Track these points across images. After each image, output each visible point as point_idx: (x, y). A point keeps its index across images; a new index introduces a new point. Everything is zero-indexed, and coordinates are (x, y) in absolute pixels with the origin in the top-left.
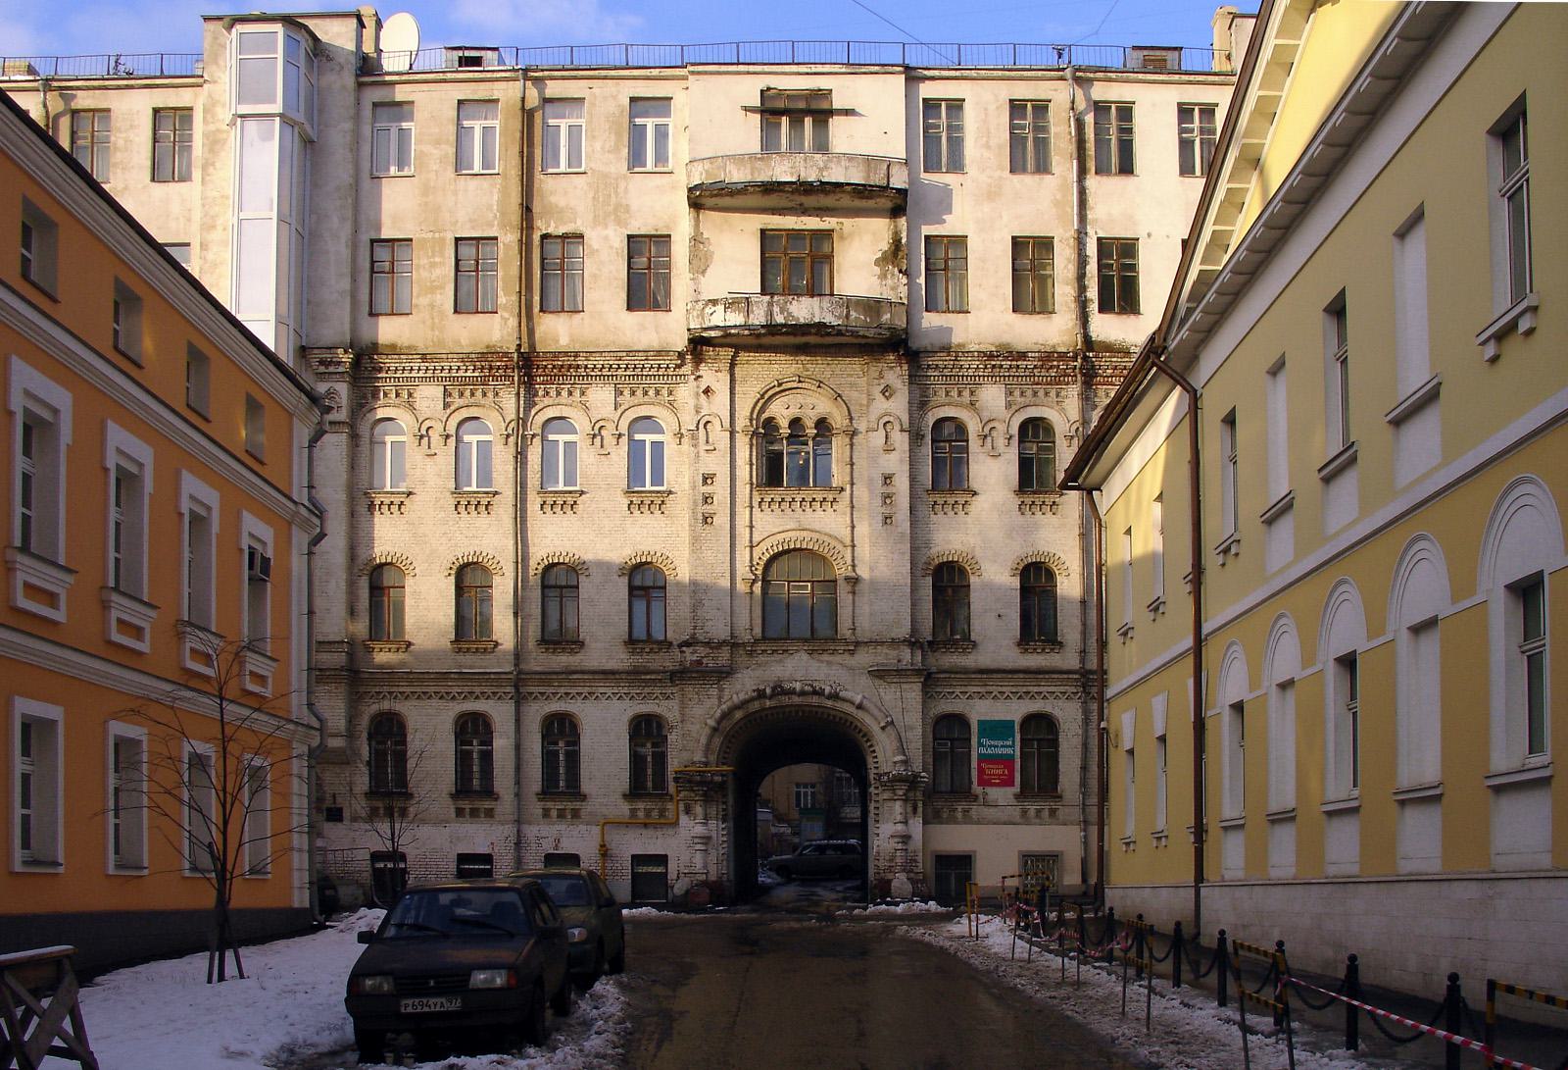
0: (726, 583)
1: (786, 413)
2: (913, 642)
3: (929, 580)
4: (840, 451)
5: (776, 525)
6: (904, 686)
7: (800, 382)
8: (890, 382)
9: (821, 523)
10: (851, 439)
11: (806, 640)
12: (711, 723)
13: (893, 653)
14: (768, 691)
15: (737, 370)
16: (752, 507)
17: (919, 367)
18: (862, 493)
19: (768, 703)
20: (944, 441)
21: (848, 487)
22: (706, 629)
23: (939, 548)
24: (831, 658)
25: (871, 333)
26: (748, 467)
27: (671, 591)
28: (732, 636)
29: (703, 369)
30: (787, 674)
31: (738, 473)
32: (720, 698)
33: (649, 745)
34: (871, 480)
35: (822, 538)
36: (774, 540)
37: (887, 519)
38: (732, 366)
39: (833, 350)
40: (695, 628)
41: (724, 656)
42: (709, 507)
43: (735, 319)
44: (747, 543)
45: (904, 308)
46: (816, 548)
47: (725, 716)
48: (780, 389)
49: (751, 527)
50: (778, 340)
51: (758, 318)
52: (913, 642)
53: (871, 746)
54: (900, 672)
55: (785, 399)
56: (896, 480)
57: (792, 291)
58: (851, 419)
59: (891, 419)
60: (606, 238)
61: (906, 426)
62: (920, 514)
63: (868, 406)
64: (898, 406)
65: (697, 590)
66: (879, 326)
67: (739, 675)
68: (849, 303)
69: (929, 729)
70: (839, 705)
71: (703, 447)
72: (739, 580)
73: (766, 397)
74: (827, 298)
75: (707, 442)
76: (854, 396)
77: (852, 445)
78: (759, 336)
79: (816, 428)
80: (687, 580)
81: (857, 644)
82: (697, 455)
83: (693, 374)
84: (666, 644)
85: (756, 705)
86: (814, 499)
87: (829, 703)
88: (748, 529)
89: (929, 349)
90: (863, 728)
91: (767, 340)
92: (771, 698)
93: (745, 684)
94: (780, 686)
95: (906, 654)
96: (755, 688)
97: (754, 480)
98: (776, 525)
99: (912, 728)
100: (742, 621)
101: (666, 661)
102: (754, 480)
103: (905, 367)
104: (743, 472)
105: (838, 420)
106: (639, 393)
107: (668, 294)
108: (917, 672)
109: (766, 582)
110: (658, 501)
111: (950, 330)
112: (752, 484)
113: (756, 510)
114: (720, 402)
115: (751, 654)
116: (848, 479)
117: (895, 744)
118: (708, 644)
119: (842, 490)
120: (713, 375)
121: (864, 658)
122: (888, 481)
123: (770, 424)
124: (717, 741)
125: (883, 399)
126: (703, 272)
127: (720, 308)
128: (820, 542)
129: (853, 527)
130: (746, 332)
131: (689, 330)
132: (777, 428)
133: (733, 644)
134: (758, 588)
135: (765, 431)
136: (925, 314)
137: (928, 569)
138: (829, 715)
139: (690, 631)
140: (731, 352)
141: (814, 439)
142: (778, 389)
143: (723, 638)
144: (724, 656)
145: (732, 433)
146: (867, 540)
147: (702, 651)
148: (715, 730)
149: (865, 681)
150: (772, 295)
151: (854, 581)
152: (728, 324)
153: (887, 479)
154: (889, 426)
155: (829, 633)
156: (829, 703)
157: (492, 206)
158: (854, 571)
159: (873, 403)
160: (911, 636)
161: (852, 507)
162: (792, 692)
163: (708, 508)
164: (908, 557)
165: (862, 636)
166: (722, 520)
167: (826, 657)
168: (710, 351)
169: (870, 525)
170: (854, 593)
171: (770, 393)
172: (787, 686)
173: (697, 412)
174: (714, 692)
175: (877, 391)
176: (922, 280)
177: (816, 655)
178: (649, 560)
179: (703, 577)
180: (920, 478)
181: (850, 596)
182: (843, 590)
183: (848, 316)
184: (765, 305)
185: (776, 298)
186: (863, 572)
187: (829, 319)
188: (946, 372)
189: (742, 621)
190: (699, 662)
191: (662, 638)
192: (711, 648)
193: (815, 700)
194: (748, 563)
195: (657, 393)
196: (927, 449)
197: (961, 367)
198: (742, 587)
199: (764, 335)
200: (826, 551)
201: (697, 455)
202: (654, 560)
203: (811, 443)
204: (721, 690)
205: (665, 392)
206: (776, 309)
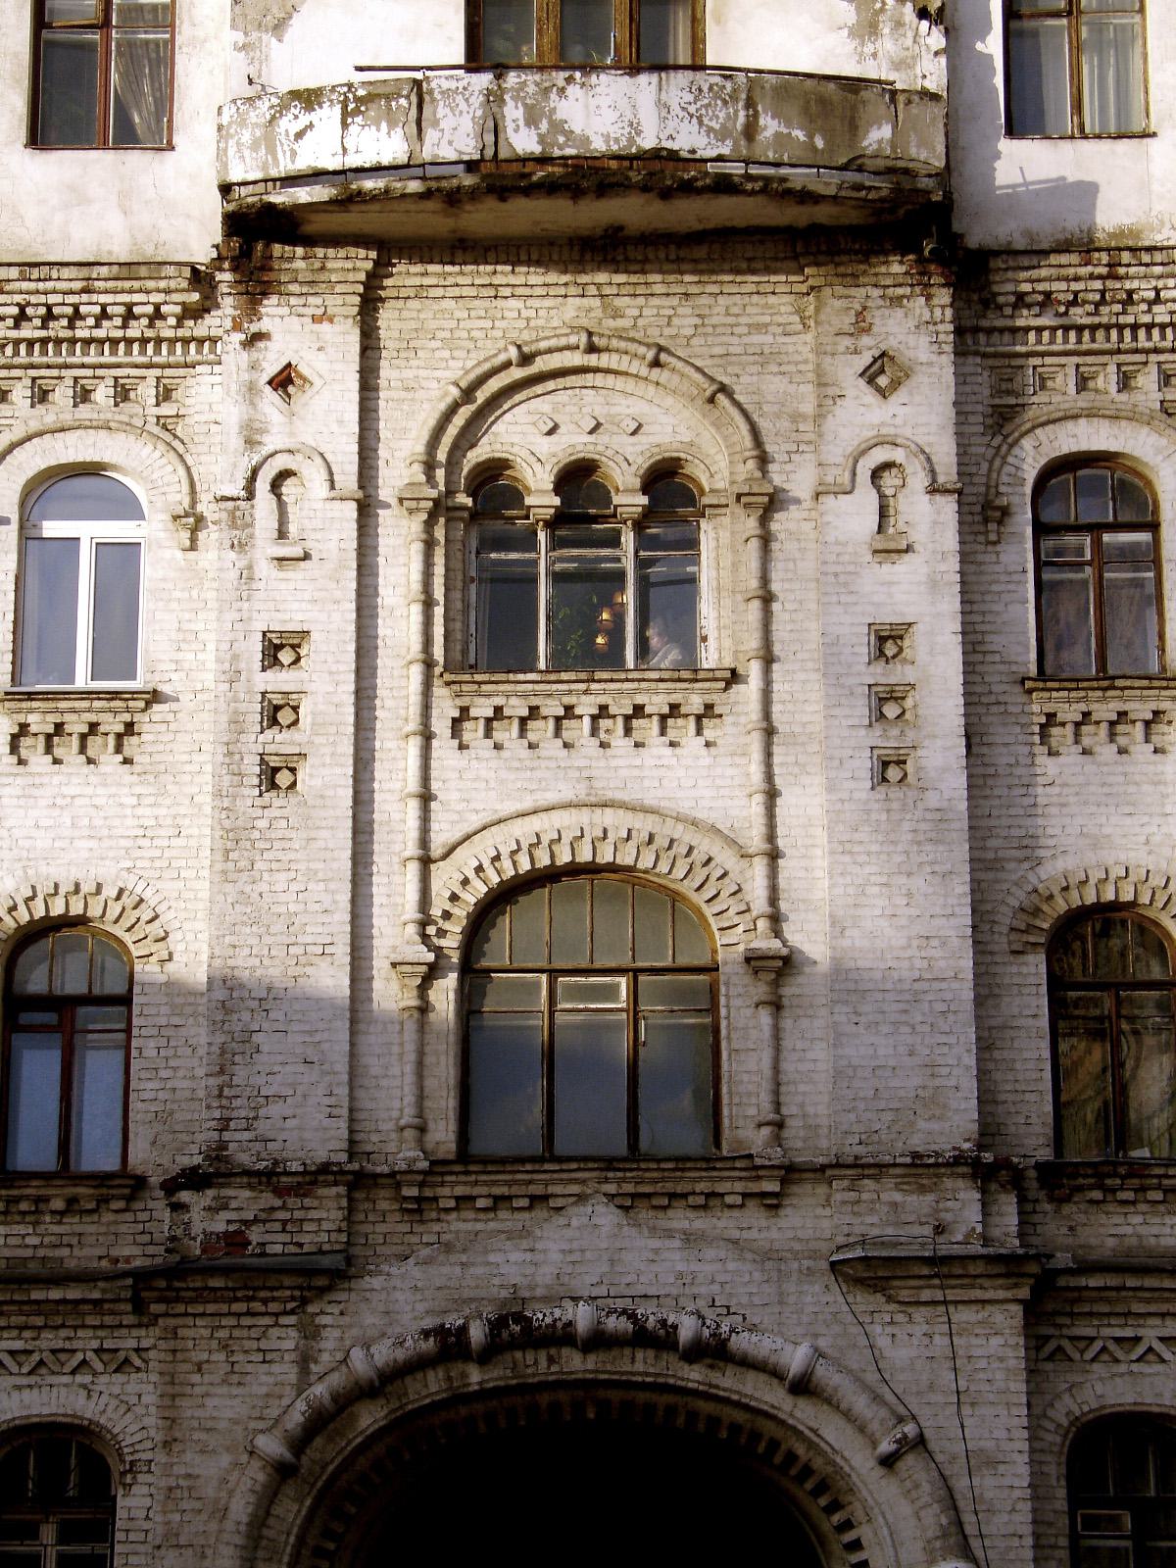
0: (332, 979)
1: (545, 446)
2: (987, 1167)
3: (1036, 966)
4: (726, 561)
5: (507, 792)
6: (963, 1316)
7: (592, 349)
8: (891, 344)
9: (668, 784)
10: (764, 520)
11: (609, 1163)
12: (272, 1446)
13: (918, 1204)
14: (477, 1333)
15: (388, 319)
16: (427, 736)
17: (989, 303)
18: (802, 697)
19: (475, 1376)
20: (1077, 529)
21: (754, 670)
22: (262, 1127)
23: (1061, 865)
24: (700, 1223)
25: (827, 183)
26: (416, 610)
27: (146, 1014)
28: (353, 1148)
29: (273, 314)
30: (545, 1276)
31: (385, 628)
32: (305, 1361)
33: (48, 1533)
34: (831, 646)
35: (666, 830)
36: (501, 839)
37: (888, 768)
38: (369, 304)
39: (701, 252)
40: (224, 1124)
41: (323, 1219)
42: (286, 735)
43: (379, 144)
44: (412, 849)
45: (938, 111)
46: (647, 862)
47: (319, 1422)
48: (528, 374)
49: (426, 798)
50: (525, 214)
51: (453, 138)
52: (987, 1167)
53: (835, 1506)
54: (943, 1267)
55: (543, 405)
56: (917, 645)
57: (577, 55)
58: (763, 460)
59: (898, 455)
61: (948, 473)
62: (1002, 758)
63: (819, 417)
64: (924, 415)
65: (235, 1007)
66: (855, 164)
67: (376, 1282)
68: (757, 89)
69: (1055, 1470)
70: (728, 1381)
71: (265, 545)
72: (380, 966)
73: (481, 396)
74: (681, 78)
75: (282, 534)
76: (771, 392)
77: (766, 540)
78: (453, 198)
79: (645, 489)
80: (200, 976)
81: (791, 1173)
82: (247, 576)
83: (237, 327)
84: (127, 1185)
85: (432, 1385)
86: (639, 711)
87: (694, 1375)
88: (414, 805)
89: (1020, 244)
90: (818, 1463)
91: (484, 218)
92: (486, 1356)
93: (393, 1310)
94: (519, 1318)
95: (964, 1207)
96: (429, 1323)
97: (438, 652)
98: (507, 792)
99: (992, 1463)
100: (391, 1100)
101: (125, 1240)
102: (438, 652)
103: (943, 296)
104: (401, 627)
105: (718, 466)
106: (62, 395)
107: (164, 103)
108: (1007, 1266)
109: (473, 975)
110: (108, 719)
111: (1087, 192)
112: (429, 664)
113: (443, 746)
114: (328, 415)
115: (418, 1209)
116: (753, 642)
117: (934, 1518)
118: (268, 1177)
119: (734, 677)
120: (310, 331)
121: (815, 1220)
122: (890, 649)
123: (493, 485)
124: (291, 1511)
125: (869, 396)
126: (279, 28)
127: (328, 116)
128: (661, 842)
129: (772, 795)
130: (414, 186)
131: (226, 189)
132: (514, 496)
133: (357, 1178)
134: (445, 993)
135: (477, 506)
136: (1006, 145)
137: (1030, 929)
138: (693, 1415)
139: (207, 1136)
140: (363, 260)
141: (639, 526)
142: (517, 373)
143: (321, 1156)
144: (325, 1214)
145: (366, 509)
146: (821, 836)
147: (245, 1201)
148: (283, 1472)
149: (820, 1297)
150: (500, 70)
151: (777, 969)
152: (353, 161)
153: (888, 640)
154: (889, 480)
155: (692, 1141)
156: (694, 1375)
158: (777, 933)
159: (837, 418)
160: (981, 1147)
161: (769, 732)
162: (562, 1337)
163: (280, 741)
164: (961, 887)
165: (801, 1145)
166: (326, 776)
167: (680, 1219)
168: (294, 260)
169: (831, 788)
170: (777, 1006)
171: (494, 384)
172: (542, 1316)
173: (251, 443)
174: (285, 1339)
175: (848, 370)
176: (993, 45)
177: (644, 1214)
178: (76, 909)
179: (260, 962)
180: (996, 642)
181: (765, 1017)
182: (743, 1017)
183: (750, 131)
184: (477, 100)
185: (512, 79)
186: (808, 936)
187: (688, 139)
188: (1078, 315)
189: (391, 1100)
190: (235, 1240)
191: (112, 1164)
192: (279, 1192)
193: (641, 1364)
194: (411, 911)
195: (122, 394)
196: (1019, 551)
197: (1129, 300)
198: (390, 994)
199: (474, 194)
200: (679, 872)
201: (247, 576)
202: (94, 911)
203: (628, 539)
204: (311, 1332)
205: (147, 391)
206: (513, 112)
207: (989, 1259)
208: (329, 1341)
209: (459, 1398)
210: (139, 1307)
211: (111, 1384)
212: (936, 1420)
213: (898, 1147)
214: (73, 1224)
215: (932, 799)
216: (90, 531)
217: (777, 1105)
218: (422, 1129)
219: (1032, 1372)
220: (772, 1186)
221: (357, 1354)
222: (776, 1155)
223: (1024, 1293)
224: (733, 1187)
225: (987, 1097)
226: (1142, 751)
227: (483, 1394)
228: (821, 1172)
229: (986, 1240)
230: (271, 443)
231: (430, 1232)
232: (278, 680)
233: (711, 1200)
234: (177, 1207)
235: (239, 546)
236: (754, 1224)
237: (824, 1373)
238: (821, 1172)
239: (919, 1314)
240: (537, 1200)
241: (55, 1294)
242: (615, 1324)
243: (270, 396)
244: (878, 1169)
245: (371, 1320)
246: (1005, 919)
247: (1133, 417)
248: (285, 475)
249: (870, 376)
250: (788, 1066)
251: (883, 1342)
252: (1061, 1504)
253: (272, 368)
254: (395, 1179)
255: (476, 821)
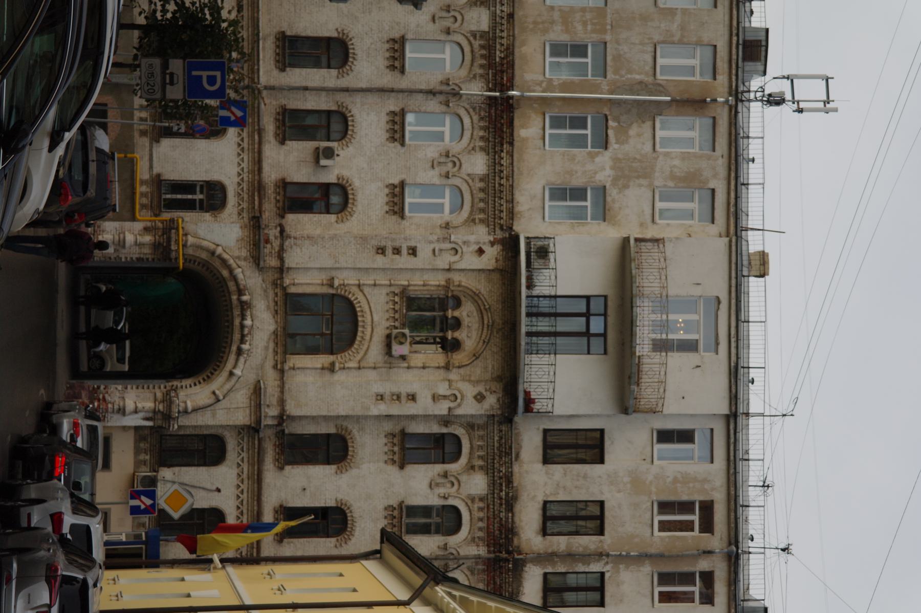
2: (282, 418)
3: (332, 430)
6: (248, 411)
12: (219, 250)
13: (274, 401)
17: (500, 423)
22: (294, 247)
24: (271, 350)
28: (289, 269)
32: (239, 258)
33: (201, 197)
40: (295, 238)
47: (224, 262)
52: (282, 418)
53: (204, 380)
56: (411, 404)
59: (459, 400)
60: (603, 169)
70: (232, 357)
71: (437, 246)
75: (441, 250)
77: (438, 368)
81: (282, 372)
82: (431, 242)
85: (232, 286)
92: (239, 299)
93: (251, 279)
95: (274, 412)
105: (458, 357)
108: (259, 421)
115: (275, 284)
118: (282, 250)
123: (458, 303)
124: (204, 255)
125: (474, 393)
133: (282, 270)
139: (293, 234)
144: (273, 262)
147: (276, 244)
148: (213, 253)
149: (251, 378)
157: (631, 74)
158: (340, 369)
162: (243, 317)
163: (389, 251)
167: (272, 345)
170: (323, 369)
173: (464, 243)
177: (273, 337)
181: (320, 366)
190: (267, 241)
193: (237, 336)
196: (436, 429)
201: (431, 242)
207: (260, 417)
208: (242, 263)
209: (229, 293)
210: (254, 217)
211: (235, 211)
212: (224, 404)
213: (287, 396)
214: (273, 201)
215: (372, 407)
216: (446, 201)
217: (298, 368)
218: (294, 284)
219: (236, 426)
220: (279, 366)
221: (240, 270)
222: (286, 368)
223: (253, 425)
224: (279, 358)
225: (301, 418)
226: (386, 458)
227: (230, 300)
228: (282, 379)
229: (265, 417)
230: (465, 249)
231: (269, 286)
232: (404, 251)
233: (276, 353)
234: (276, 227)
235: (438, 240)
236: (270, 363)
237: (234, 379)
238: (282, 379)
239: (248, 401)
240: (276, 312)
241: (256, 198)
242: (246, 331)
243: (477, 247)
244: (282, 392)
245: (248, 273)
246: (345, 424)
247: (470, 459)
248: (457, 251)
249: (480, 394)
250: (308, 371)
251: (242, 392)
252: (205, 432)
253: (484, 248)
254: (282, 278)
255: (369, 297)
